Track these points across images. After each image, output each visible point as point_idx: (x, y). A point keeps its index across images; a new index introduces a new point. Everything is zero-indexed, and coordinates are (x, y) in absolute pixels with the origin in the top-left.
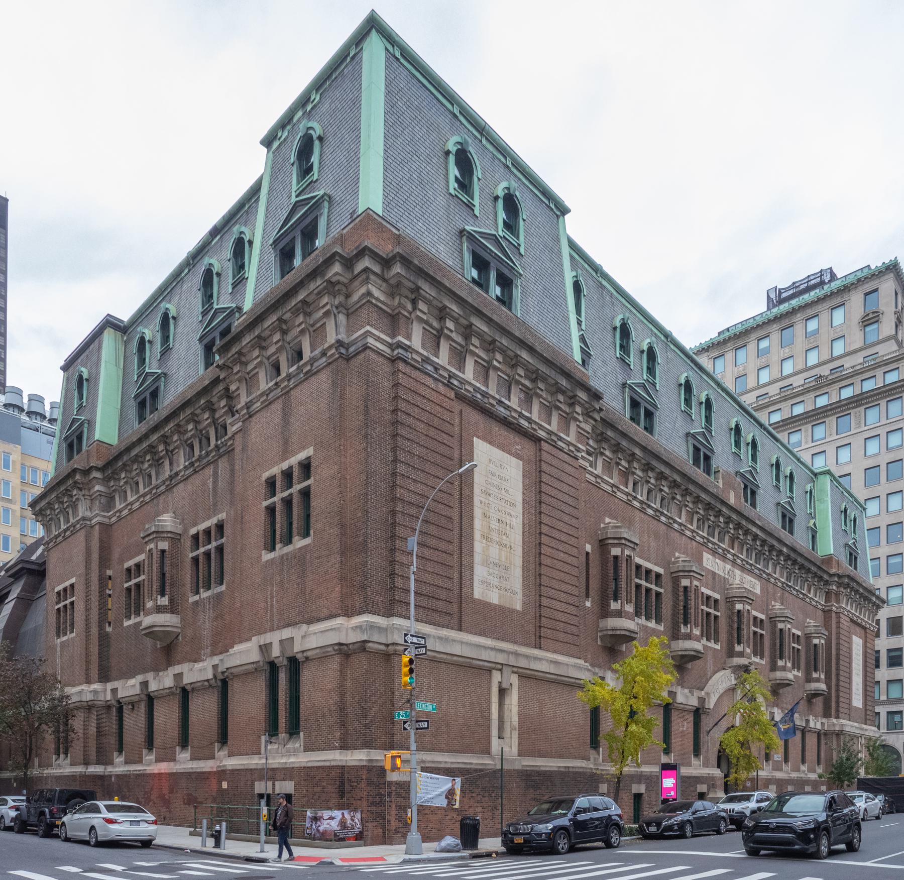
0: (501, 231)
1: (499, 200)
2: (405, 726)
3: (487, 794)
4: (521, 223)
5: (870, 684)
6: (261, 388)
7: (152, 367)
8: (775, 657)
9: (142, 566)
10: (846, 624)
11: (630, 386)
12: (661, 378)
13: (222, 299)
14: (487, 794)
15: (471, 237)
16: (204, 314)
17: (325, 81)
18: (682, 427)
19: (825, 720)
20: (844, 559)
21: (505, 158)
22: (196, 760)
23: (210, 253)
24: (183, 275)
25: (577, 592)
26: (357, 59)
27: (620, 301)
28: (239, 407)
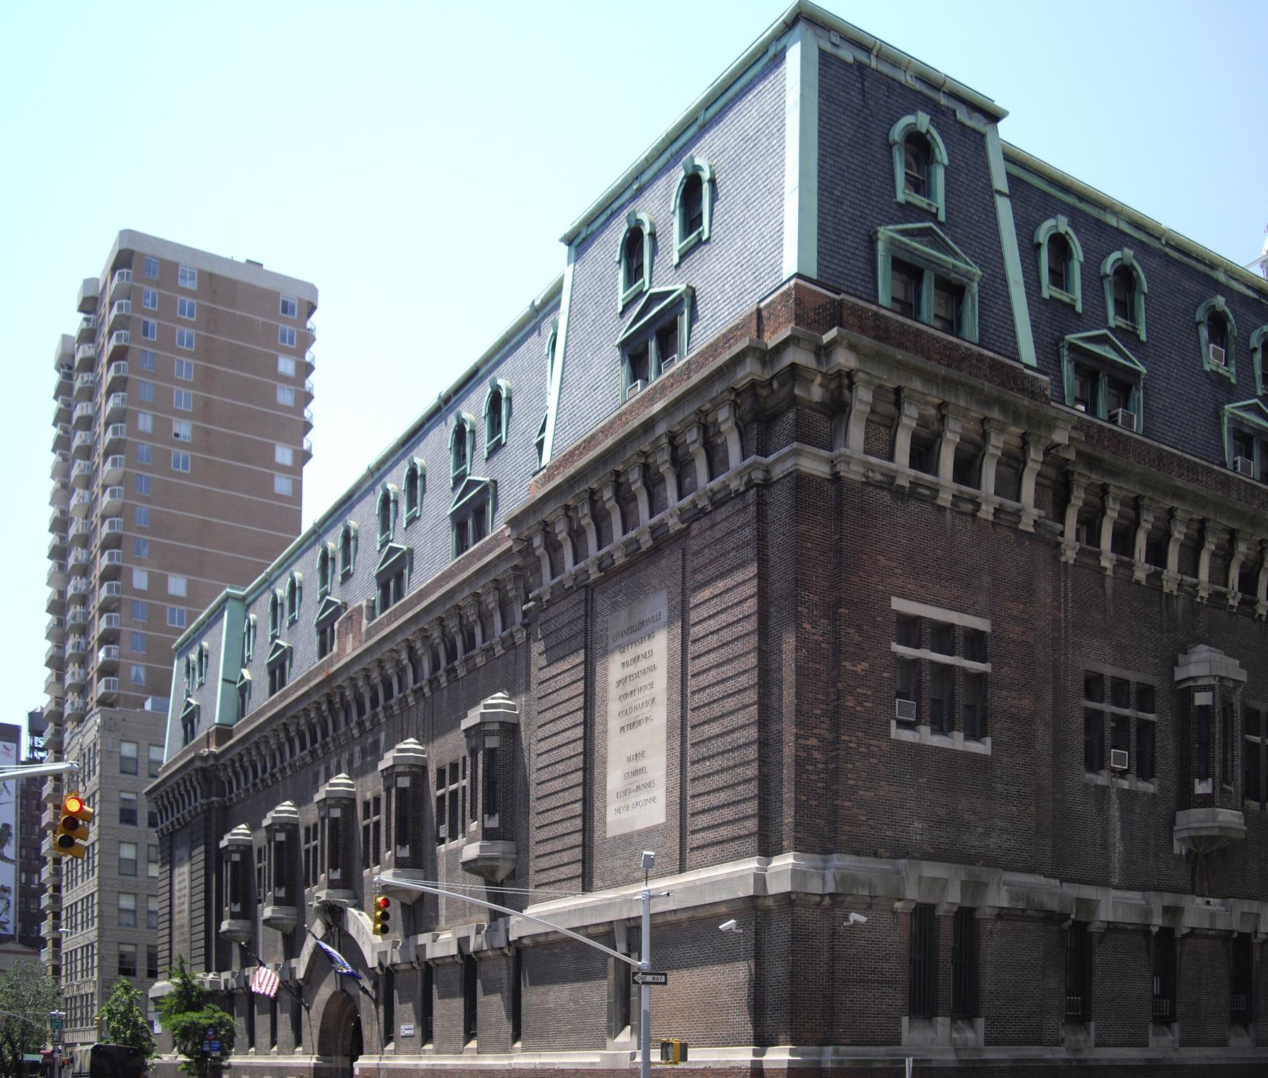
2: (636, 978)
7: (478, 473)
8: (1010, 885)
9: (460, 795)
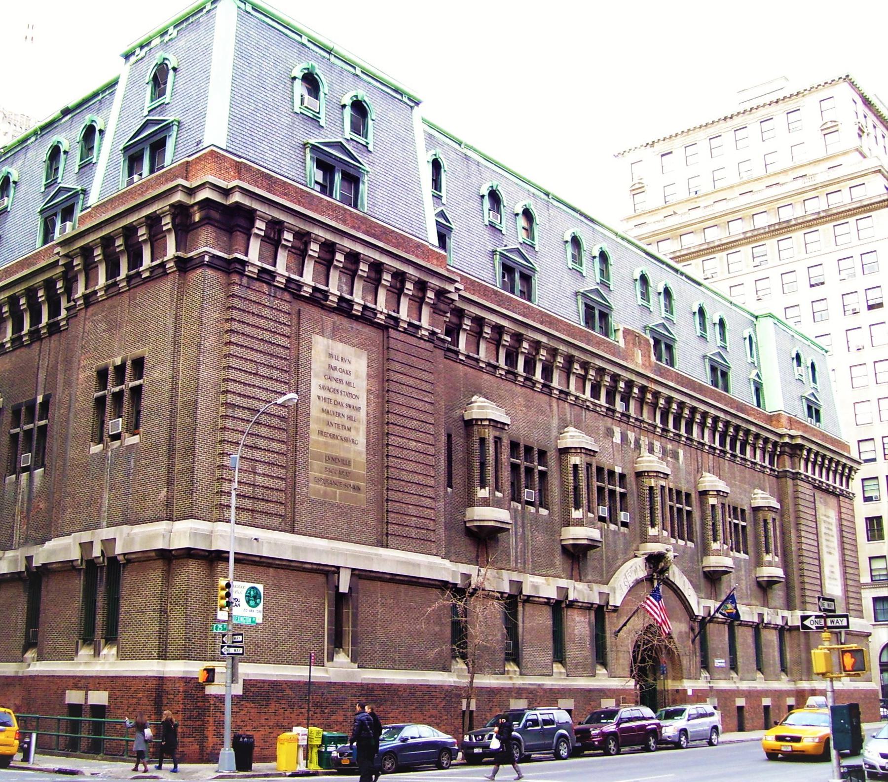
0: (348, 133)
1: (347, 107)
3: (318, 710)
4: (370, 123)
5: (848, 565)
6: (99, 283)
10: (808, 492)
11: (500, 253)
12: (541, 238)
13: (67, 175)
14: (318, 710)
15: (314, 148)
16: (47, 186)
17: (182, 22)
18: (571, 285)
19: (786, 613)
20: (801, 413)
21: (355, 68)
22: (727, 731)
23: (58, 129)
24: (29, 142)
25: (433, 482)
26: (211, 13)
27: (489, 168)
28: (76, 296)
